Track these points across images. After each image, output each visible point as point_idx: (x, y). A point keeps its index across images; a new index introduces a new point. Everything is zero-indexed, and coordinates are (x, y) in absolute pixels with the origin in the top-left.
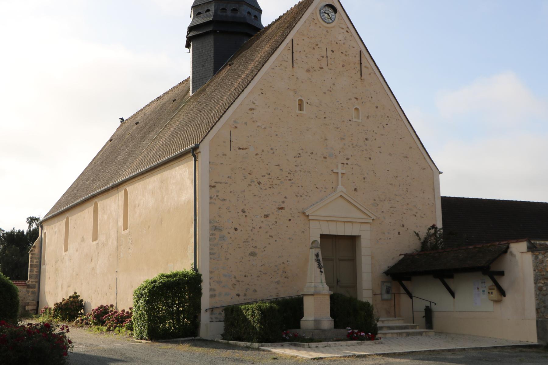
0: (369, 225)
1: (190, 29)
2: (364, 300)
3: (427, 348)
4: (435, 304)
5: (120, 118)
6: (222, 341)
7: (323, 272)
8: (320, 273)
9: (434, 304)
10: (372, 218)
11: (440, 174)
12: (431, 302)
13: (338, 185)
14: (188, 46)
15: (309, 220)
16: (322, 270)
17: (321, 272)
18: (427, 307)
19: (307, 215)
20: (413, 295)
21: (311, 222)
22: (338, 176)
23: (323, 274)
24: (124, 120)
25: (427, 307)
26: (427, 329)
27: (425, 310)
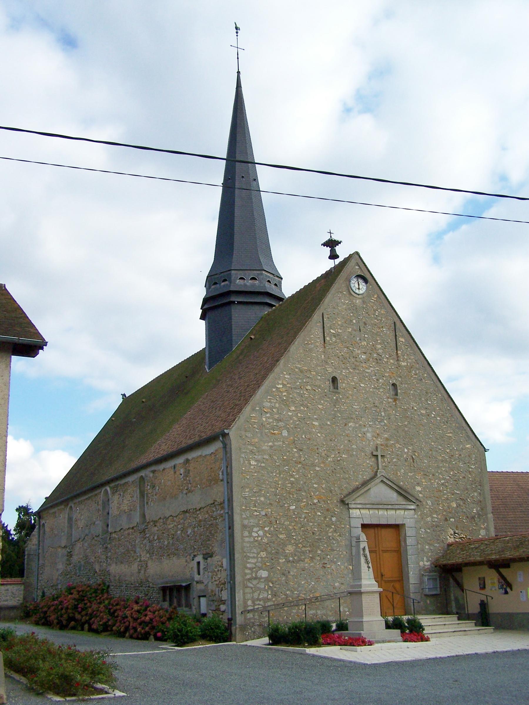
0: (413, 511)
1: (206, 301)
2: (22, 441)
3: (432, 655)
4: (492, 598)
5: (122, 394)
6: (97, 648)
7: (371, 567)
8: (368, 568)
9: (491, 598)
10: (417, 504)
11: (486, 451)
12: (487, 596)
13: (378, 469)
14: (203, 317)
15: (349, 508)
16: (370, 565)
17: (369, 567)
18: (482, 601)
19: (347, 503)
20: (465, 587)
21: (351, 511)
22: (377, 459)
23: (371, 570)
24: (126, 396)
25: (482, 601)
26: (483, 626)
27: (480, 604)
